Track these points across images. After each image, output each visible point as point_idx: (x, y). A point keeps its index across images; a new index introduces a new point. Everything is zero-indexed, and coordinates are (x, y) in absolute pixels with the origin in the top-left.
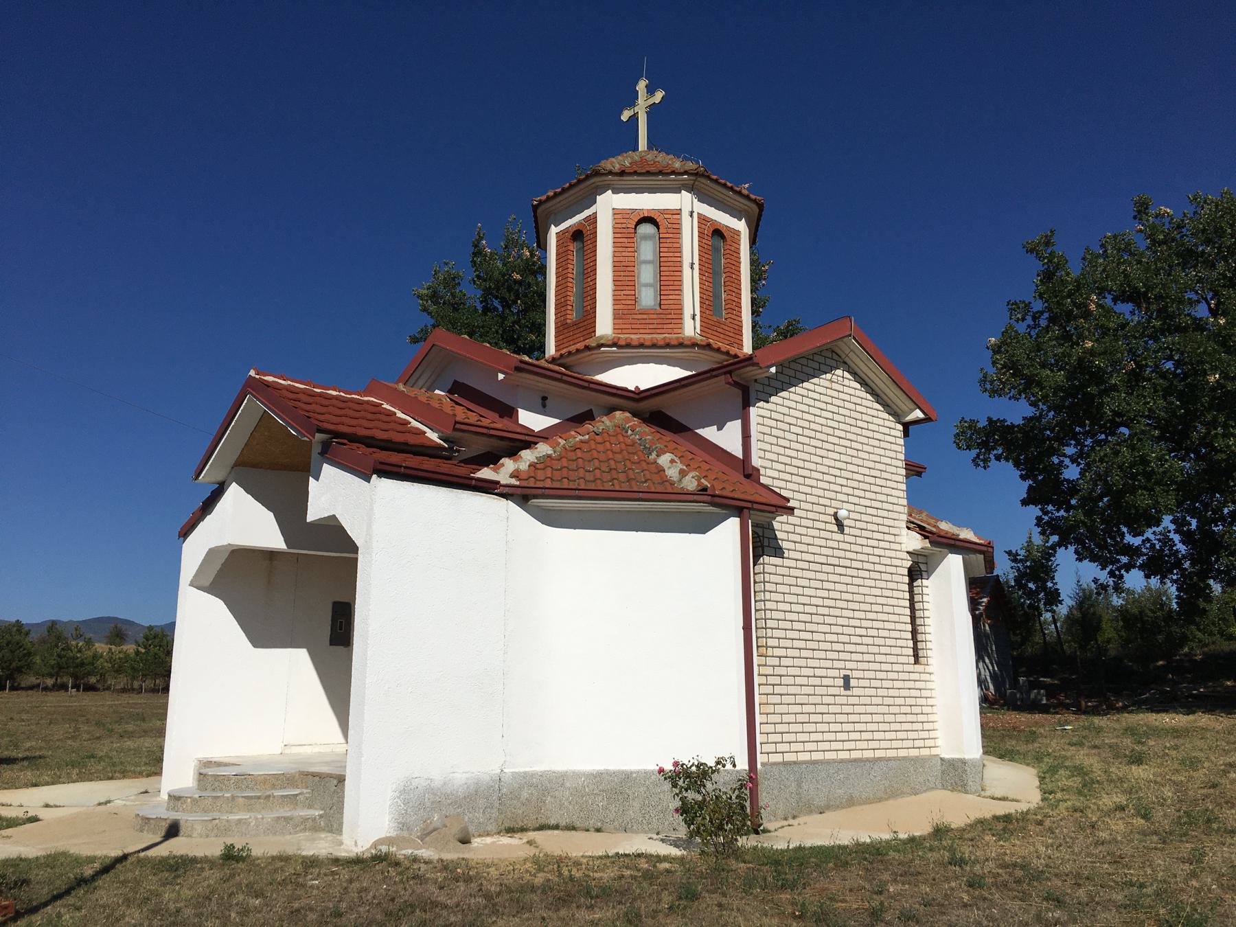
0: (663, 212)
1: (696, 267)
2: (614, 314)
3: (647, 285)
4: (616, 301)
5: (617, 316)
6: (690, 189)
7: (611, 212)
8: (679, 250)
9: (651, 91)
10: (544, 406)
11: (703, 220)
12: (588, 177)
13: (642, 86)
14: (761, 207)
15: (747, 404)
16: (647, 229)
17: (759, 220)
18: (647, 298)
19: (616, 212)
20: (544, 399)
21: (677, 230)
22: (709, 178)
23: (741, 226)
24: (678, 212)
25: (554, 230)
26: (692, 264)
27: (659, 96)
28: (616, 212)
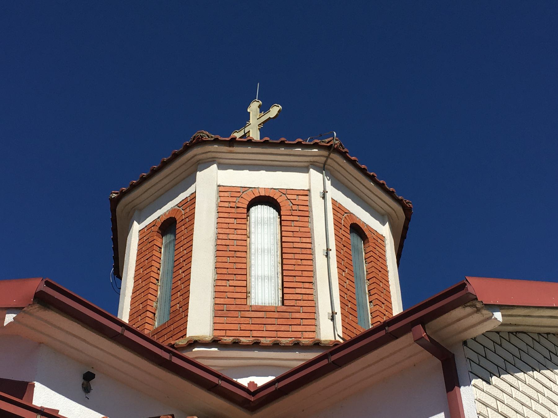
0: (284, 192)
1: (333, 254)
2: (215, 311)
3: (263, 278)
4: (218, 293)
5: (219, 312)
6: (322, 168)
7: (215, 188)
8: (309, 235)
9: (264, 109)
10: (87, 389)
11: (338, 208)
12: (187, 148)
13: (254, 108)
14: (407, 210)
15: (453, 382)
16: (262, 214)
17: (406, 228)
18: (264, 291)
19: (222, 190)
20: (88, 377)
21: (305, 213)
22: (344, 155)
23: (385, 230)
24: (307, 193)
25: (136, 227)
26: (328, 250)
27: (274, 111)
28: (222, 190)
